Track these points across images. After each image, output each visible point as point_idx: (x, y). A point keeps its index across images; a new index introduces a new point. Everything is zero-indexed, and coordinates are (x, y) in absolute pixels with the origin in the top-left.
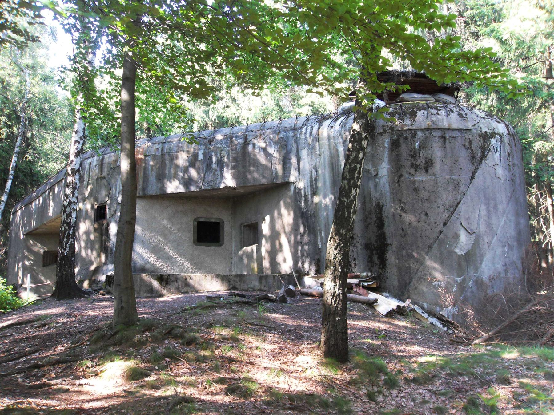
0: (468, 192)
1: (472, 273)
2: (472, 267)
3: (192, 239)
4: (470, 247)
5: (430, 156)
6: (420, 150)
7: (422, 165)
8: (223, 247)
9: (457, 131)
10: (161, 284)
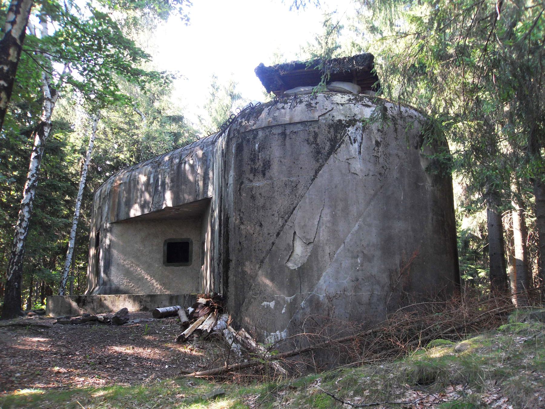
0: (307, 195)
1: (305, 291)
2: (306, 284)
3: (162, 260)
4: (306, 260)
5: (268, 157)
6: (259, 152)
7: (260, 169)
8: (191, 267)
9: (299, 125)
10: (78, 305)
